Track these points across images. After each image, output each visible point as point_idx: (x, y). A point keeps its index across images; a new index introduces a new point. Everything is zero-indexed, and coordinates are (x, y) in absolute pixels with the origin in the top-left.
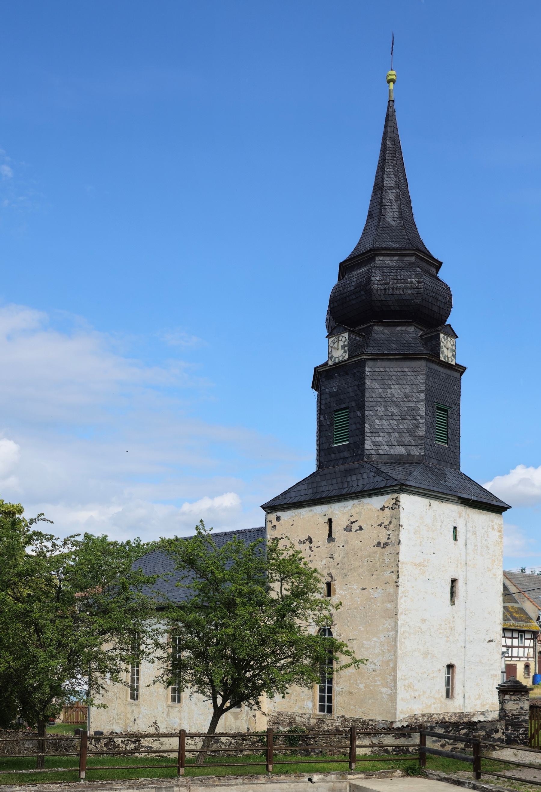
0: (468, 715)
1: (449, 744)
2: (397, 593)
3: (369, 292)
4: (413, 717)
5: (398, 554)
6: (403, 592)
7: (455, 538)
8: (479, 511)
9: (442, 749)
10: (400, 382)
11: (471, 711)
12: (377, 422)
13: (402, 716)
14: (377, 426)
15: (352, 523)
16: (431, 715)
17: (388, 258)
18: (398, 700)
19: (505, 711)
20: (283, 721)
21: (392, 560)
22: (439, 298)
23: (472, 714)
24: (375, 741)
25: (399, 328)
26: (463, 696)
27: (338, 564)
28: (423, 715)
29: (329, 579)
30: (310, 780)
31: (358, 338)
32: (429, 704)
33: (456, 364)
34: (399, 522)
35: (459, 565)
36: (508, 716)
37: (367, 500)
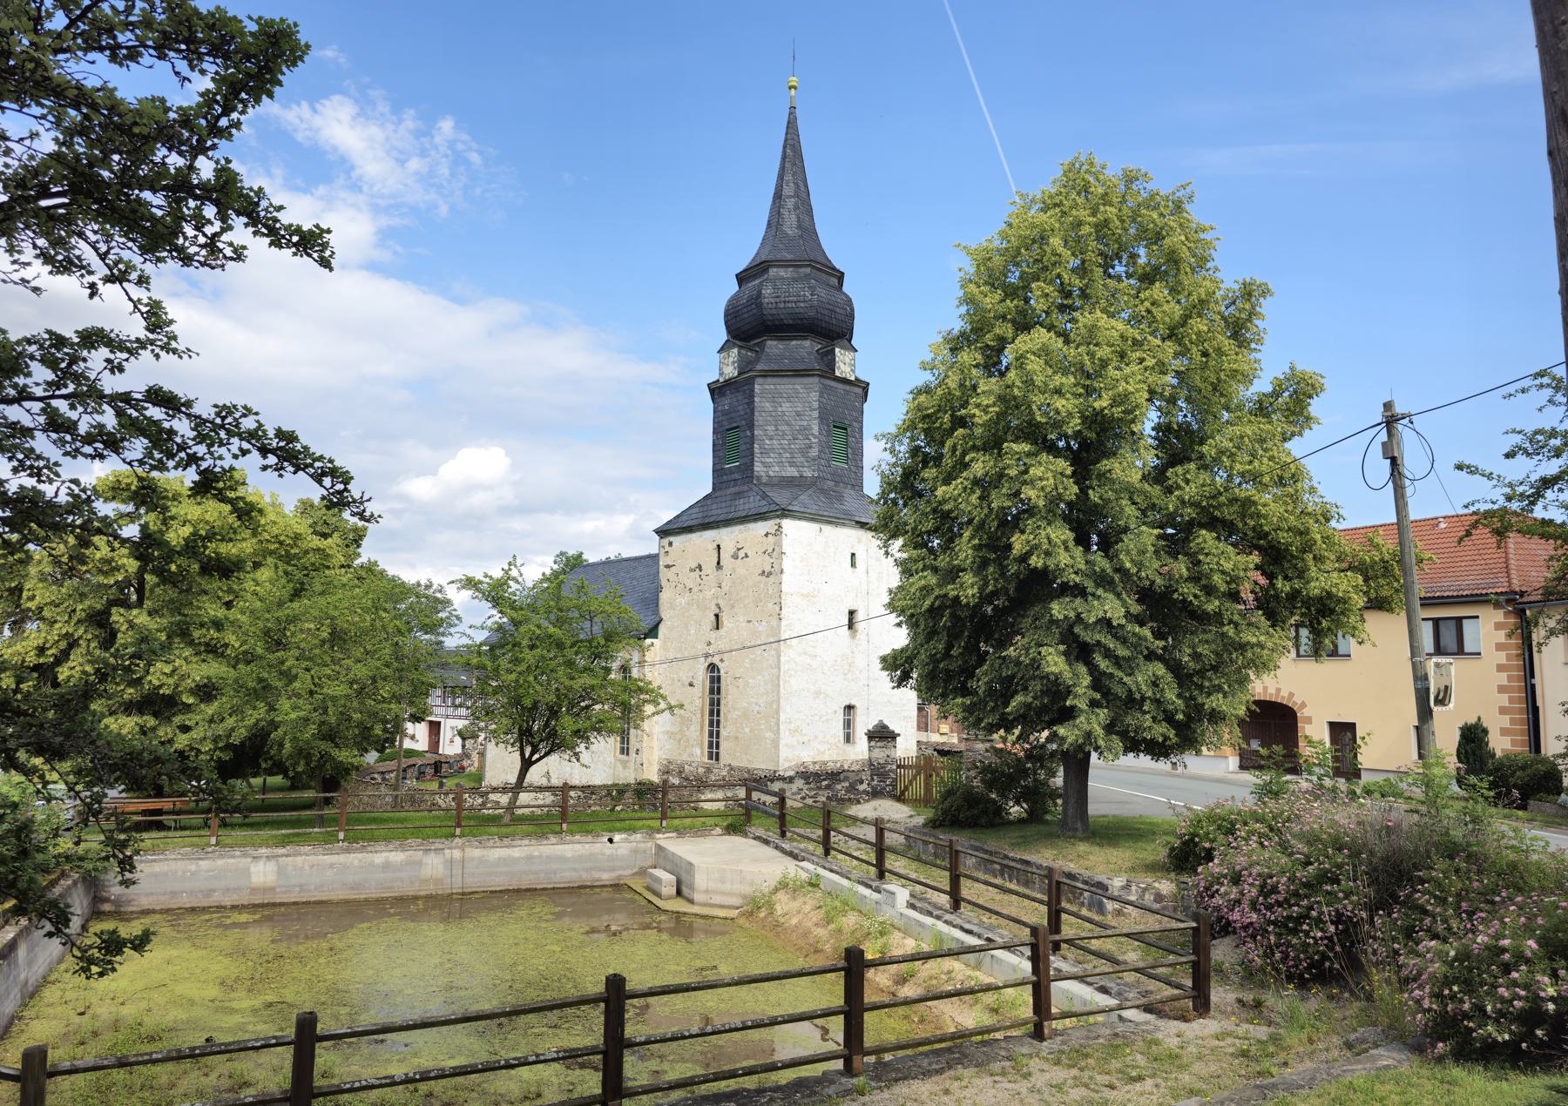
3: (760, 306)
7: (853, 565)
13: (787, 765)
16: (825, 763)
24: (729, 794)
29: (1483, 535)
30: (611, 841)
37: (752, 526)
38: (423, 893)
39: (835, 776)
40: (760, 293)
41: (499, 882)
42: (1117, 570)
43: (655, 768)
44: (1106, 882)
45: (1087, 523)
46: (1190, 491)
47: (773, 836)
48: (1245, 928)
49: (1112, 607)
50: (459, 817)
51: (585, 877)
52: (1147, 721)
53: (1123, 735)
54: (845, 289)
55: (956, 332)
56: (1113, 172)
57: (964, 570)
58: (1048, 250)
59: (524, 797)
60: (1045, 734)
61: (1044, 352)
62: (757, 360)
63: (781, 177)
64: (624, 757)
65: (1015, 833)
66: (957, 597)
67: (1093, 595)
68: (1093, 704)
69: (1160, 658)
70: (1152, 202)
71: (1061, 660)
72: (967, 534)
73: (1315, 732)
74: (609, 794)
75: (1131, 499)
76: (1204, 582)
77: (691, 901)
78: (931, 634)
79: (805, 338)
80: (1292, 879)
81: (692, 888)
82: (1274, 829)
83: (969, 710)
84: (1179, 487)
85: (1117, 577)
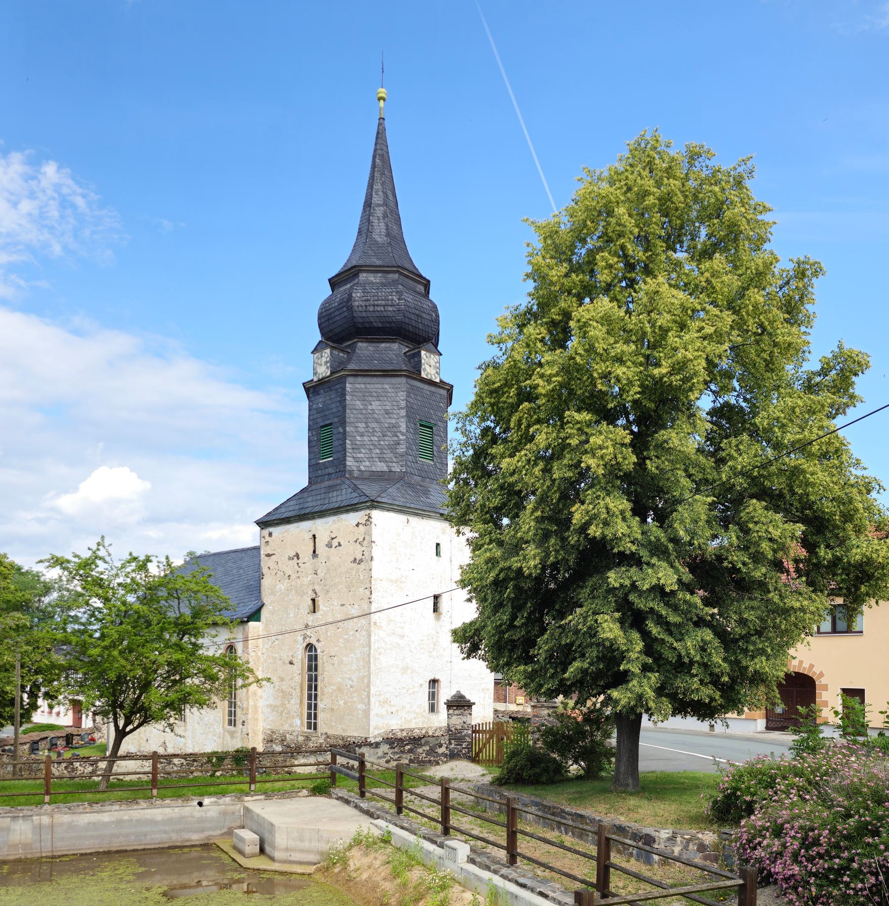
3: (350, 308)
7: (438, 554)
9: (387, 765)
10: (381, 398)
12: (358, 438)
13: (376, 732)
14: (358, 443)
15: (333, 539)
16: (412, 730)
17: (372, 275)
22: (424, 315)
25: (383, 345)
29: (314, 596)
30: (200, 804)
31: (341, 354)
33: (441, 381)
37: (344, 517)
38: (11, 858)
39: (416, 741)
40: (350, 296)
41: (89, 845)
42: (671, 540)
43: (261, 737)
44: (653, 834)
45: (647, 495)
46: (743, 461)
47: (354, 797)
48: (787, 879)
49: (667, 575)
50: (47, 784)
51: (175, 838)
52: (695, 683)
53: (673, 697)
54: (431, 296)
55: (523, 308)
56: (677, 151)
57: (527, 542)
58: (613, 220)
59: (122, 766)
60: (602, 697)
61: (606, 320)
62: (349, 360)
63: (371, 186)
64: (232, 728)
65: (572, 789)
66: (521, 568)
67: (648, 564)
68: (646, 668)
69: (709, 625)
70: (714, 178)
71: (616, 627)
72: (530, 507)
73: (829, 703)
74: (209, 761)
75: (686, 470)
76: (752, 550)
77: (272, 859)
78: (498, 607)
79: (393, 341)
80: (833, 832)
81: (273, 847)
82: (813, 784)
83: (531, 676)
84: (732, 457)
85: (671, 546)
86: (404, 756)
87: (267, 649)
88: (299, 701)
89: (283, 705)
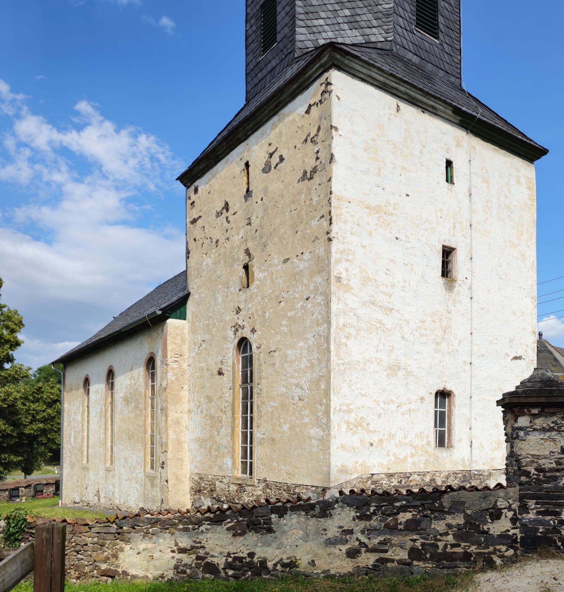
0: (480, 475)
1: (369, 550)
2: (328, 252)
4: (369, 478)
5: (330, 180)
6: (342, 252)
7: (449, 179)
8: (492, 146)
11: (486, 468)
16: (407, 476)
18: (333, 448)
19: (518, 461)
20: (205, 489)
21: (322, 196)
23: (486, 474)
26: (469, 444)
27: (256, 231)
28: (390, 476)
32: (402, 457)
34: (331, 121)
35: (458, 225)
36: (527, 474)
39: (430, 500)
43: (187, 486)
86: (395, 539)
87: (194, 358)
88: (230, 430)
89: (212, 437)
